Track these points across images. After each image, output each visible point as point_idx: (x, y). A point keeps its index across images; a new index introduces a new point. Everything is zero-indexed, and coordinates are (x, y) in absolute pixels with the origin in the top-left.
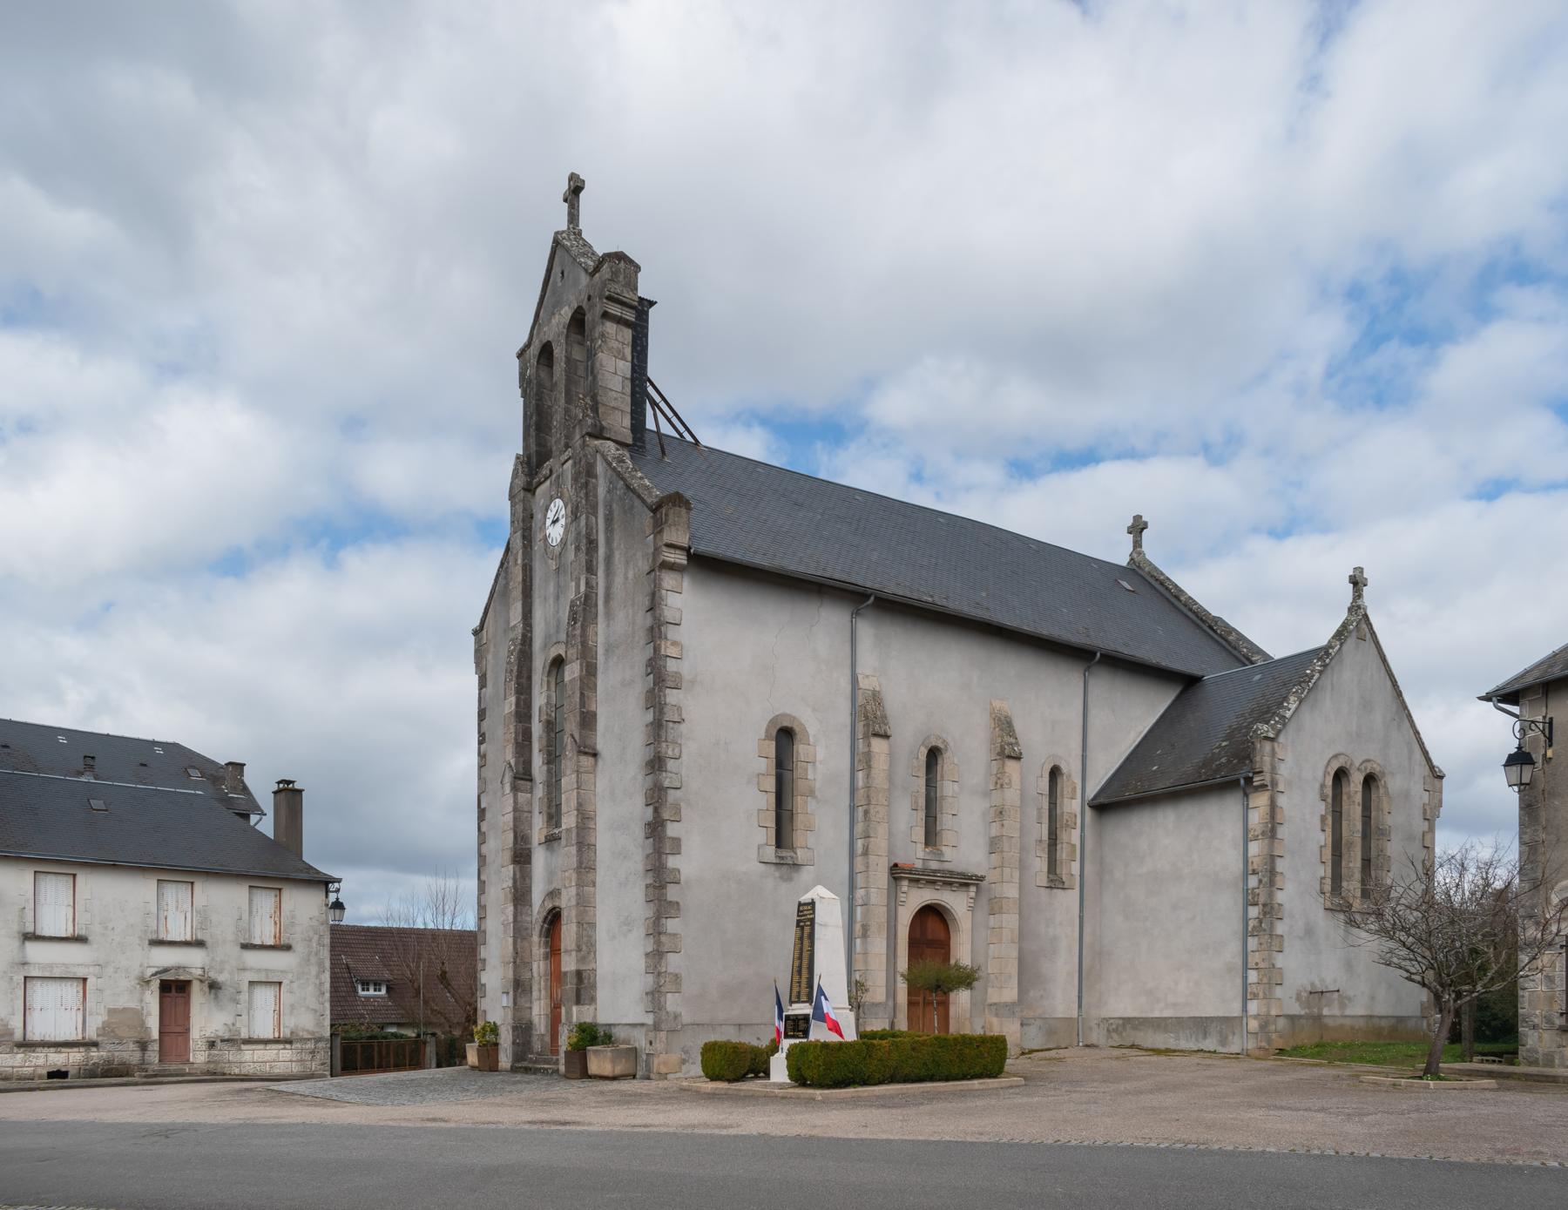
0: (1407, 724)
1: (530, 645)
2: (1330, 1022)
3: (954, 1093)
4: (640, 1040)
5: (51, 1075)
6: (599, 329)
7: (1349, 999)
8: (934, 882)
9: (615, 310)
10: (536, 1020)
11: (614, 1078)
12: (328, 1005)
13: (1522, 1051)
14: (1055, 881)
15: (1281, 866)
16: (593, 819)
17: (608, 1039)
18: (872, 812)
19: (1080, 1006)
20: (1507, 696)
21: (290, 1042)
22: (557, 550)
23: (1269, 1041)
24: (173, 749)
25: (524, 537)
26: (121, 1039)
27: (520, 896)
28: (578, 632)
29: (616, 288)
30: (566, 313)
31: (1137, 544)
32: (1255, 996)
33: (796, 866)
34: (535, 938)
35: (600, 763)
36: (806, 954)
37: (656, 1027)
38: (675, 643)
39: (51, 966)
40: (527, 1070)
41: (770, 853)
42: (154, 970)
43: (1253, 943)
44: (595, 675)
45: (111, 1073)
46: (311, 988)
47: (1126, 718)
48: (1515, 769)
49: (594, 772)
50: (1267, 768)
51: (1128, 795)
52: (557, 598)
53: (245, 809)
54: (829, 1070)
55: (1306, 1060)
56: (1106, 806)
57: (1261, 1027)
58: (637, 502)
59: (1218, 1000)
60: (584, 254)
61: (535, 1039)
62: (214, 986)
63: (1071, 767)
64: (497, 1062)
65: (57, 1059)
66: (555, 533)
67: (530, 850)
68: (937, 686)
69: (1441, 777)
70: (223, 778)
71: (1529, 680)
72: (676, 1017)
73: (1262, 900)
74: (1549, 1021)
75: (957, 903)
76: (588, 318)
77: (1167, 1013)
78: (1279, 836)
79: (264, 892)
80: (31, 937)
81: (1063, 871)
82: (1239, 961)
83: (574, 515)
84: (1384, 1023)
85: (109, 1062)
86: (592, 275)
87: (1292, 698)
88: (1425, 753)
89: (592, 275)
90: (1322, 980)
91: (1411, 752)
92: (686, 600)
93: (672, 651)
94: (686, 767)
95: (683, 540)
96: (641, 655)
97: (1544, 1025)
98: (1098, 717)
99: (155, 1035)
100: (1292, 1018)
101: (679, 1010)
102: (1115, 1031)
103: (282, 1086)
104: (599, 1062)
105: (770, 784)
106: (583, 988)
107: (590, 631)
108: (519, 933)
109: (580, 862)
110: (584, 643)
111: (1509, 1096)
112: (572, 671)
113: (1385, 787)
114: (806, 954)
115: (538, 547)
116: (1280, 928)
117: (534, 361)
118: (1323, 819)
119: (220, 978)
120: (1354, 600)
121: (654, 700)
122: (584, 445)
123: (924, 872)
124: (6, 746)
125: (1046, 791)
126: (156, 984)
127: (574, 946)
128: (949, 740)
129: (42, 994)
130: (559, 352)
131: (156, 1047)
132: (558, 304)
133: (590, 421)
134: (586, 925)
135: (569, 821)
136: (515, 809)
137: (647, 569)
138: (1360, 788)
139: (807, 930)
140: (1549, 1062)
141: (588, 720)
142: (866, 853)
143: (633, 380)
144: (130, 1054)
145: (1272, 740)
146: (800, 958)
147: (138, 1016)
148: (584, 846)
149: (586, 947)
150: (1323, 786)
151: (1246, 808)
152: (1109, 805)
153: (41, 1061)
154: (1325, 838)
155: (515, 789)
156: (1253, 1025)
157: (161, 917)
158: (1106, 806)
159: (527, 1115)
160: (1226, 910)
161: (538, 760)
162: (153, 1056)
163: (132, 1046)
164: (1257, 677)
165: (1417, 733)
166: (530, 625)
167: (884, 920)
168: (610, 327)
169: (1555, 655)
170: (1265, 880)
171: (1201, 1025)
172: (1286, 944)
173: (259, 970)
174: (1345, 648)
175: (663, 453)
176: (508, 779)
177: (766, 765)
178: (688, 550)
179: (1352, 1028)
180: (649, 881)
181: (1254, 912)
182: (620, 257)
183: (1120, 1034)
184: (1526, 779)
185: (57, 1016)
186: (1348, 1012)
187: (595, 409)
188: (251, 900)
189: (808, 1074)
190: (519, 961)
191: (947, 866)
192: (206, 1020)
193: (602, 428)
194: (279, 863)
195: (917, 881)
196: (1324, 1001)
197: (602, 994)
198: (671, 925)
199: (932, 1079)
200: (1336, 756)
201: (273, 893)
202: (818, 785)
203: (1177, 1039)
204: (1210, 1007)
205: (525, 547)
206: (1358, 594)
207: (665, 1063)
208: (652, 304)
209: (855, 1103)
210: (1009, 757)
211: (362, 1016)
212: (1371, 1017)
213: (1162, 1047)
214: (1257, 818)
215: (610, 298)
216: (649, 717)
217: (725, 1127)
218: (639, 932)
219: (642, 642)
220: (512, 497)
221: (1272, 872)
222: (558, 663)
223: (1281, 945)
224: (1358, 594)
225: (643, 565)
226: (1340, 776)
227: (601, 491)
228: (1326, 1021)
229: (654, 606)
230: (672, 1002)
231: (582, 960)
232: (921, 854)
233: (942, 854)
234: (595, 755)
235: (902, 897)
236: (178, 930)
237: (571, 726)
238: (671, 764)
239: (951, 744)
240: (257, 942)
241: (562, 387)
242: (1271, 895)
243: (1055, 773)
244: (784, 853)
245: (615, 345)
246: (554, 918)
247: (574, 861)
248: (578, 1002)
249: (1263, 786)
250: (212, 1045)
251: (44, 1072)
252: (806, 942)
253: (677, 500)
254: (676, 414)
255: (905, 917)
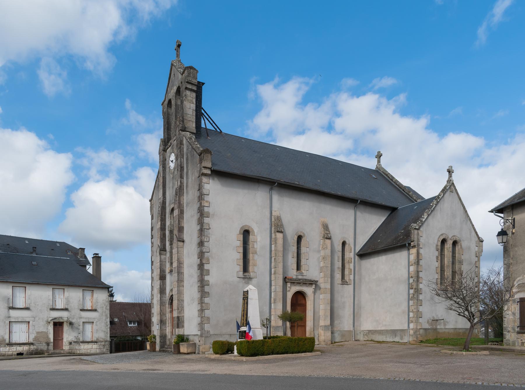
0: (469, 222)
1: (165, 204)
2: (440, 331)
3: (257, 360)
4: (196, 340)
5: (18, 354)
6: (184, 93)
7: (447, 322)
8: (300, 283)
9: (189, 86)
10: (167, 334)
11: (188, 354)
12: (109, 330)
13: (504, 340)
14: (344, 282)
15: (421, 274)
16: (183, 264)
17: (187, 340)
18: (277, 259)
19: (354, 326)
20: (499, 210)
21: (96, 342)
22: (173, 171)
23: (417, 338)
24: (63, 244)
25: (163, 167)
26: (41, 342)
27: (162, 291)
28: (177, 199)
29: (190, 79)
30: (175, 88)
31: (379, 161)
32: (412, 322)
33: (250, 278)
34: (167, 305)
35: (185, 244)
36: (245, 309)
37: (201, 336)
38: (207, 202)
39: (18, 318)
40: (164, 351)
41: (241, 274)
42: (51, 319)
43: (411, 303)
44: (183, 214)
45: (38, 354)
46: (103, 324)
47: (371, 223)
48: (501, 237)
49: (183, 247)
50: (416, 239)
51: (369, 251)
52: (173, 188)
53: (84, 264)
54: (253, 349)
55: (429, 345)
56: (363, 254)
57: (414, 333)
58: (195, 153)
59: (400, 323)
60: (180, 68)
61: (167, 340)
62: (71, 324)
63: (350, 241)
64: (155, 348)
65: (20, 349)
66: (172, 165)
67: (165, 275)
68: (301, 214)
69: (482, 241)
70: (78, 254)
71: (506, 204)
72: (208, 332)
73: (414, 287)
74: (514, 329)
75: (308, 290)
76: (181, 90)
77: (383, 328)
78: (420, 264)
79: (87, 291)
80: (12, 308)
81: (346, 278)
82: (407, 309)
83: (177, 159)
84: (460, 331)
85: (37, 350)
86: (182, 74)
87: (425, 214)
88: (476, 233)
89: (182, 74)
90: (437, 316)
91: (471, 232)
92: (213, 187)
93: (206, 204)
94: (211, 245)
95: (209, 165)
96: (196, 206)
97: (512, 331)
98: (359, 223)
99: (52, 340)
100: (426, 330)
101: (209, 329)
102: (366, 335)
103: (82, 357)
104: (183, 348)
105: (241, 250)
106: (179, 322)
107: (182, 198)
108: (162, 304)
109: (178, 279)
110: (179, 203)
111: (494, 358)
112: (176, 212)
113: (461, 245)
114: (245, 309)
115: (167, 170)
116: (421, 297)
117: (166, 106)
118: (437, 257)
119: (73, 321)
120: (449, 178)
121: (201, 222)
122: (179, 134)
123: (296, 280)
124: (8, 245)
125: (341, 250)
126: (52, 324)
127: (176, 308)
128: (305, 233)
129: (16, 327)
130: (173, 102)
131: (52, 344)
132: (173, 86)
133: (181, 125)
134: (181, 301)
135: (175, 265)
136: (160, 261)
137: (198, 176)
138: (451, 246)
139: (246, 301)
140: (514, 344)
141: (181, 229)
142: (275, 273)
143: (196, 111)
144: (44, 347)
145: (418, 229)
146: (244, 311)
147: (46, 334)
148: (180, 273)
149: (181, 309)
150: (437, 245)
151: (409, 254)
152: (364, 254)
153: (15, 350)
154: (437, 264)
155: (160, 254)
156: (412, 332)
157: (54, 301)
158: (363, 254)
159: (145, 367)
160: (402, 292)
161: (168, 243)
162: (51, 347)
163: (44, 344)
164: (416, 207)
165: (473, 225)
166: (165, 197)
167: (281, 296)
168: (188, 93)
169: (516, 195)
170: (415, 280)
171: (394, 332)
172: (423, 303)
173: (86, 318)
174: (445, 196)
175: (208, 136)
176: (158, 251)
177: (239, 243)
178: (210, 169)
179: (448, 333)
180: (199, 285)
181: (412, 291)
182: (191, 68)
183: (367, 336)
184: (505, 241)
185: (20, 334)
186: (447, 327)
187: (183, 121)
188: (83, 295)
189: (242, 352)
190: (162, 314)
191: (305, 277)
192: (68, 336)
193: (185, 128)
194: (95, 283)
195: (294, 283)
196: (438, 323)
197: (186, 325)
198: (206, 300)
199: (287, 353)
200: (442, 235)
201: (91, 292)
202: (258, 250)
203: (386, 337)
204: (397, 326)
205: (163, 170)
206: (450, 176)
207: (204, 348)
208: (203, 84)
209: (256, 362)
210: (327, 238)
211: (129, 333)
212: (456, 329)
213: (381, 340)
214: (413, 257)
215: (188, 82)
216: (199, 227)
217: (204, 371)
218: (196, 302)
219: (197, 201)
220: (159, 153)
221: (418, 277)
222: (173, 210)
223: (421, 303)
224: (450, 176)
225: (197, 175)
226: (444, 242)
227: (185, 150)
228: (438, 330)
229: (200, 189)
230: (207, 327)
231: (179, 313)
232: (295, 273)
233: (303, 273)
234: (183, 241)
235: (288, 289)
236: (60, 305)
237: (176, 232)
238: (206, 244)
239: (306, 234)
240: (86, 309)
241: (174, 114)
242: (417, 285)
243: (344, 244)
244: (246, 274)
245: (190, 98)
246: (171, 299)
247: (176, 278)
248: (178, 327)
249: (414, 247)
250: (70, 343)
251: (16, 353)
252: (246, 305)
253: (206, 151)
254: (214, 122)
255: (290, 295)
